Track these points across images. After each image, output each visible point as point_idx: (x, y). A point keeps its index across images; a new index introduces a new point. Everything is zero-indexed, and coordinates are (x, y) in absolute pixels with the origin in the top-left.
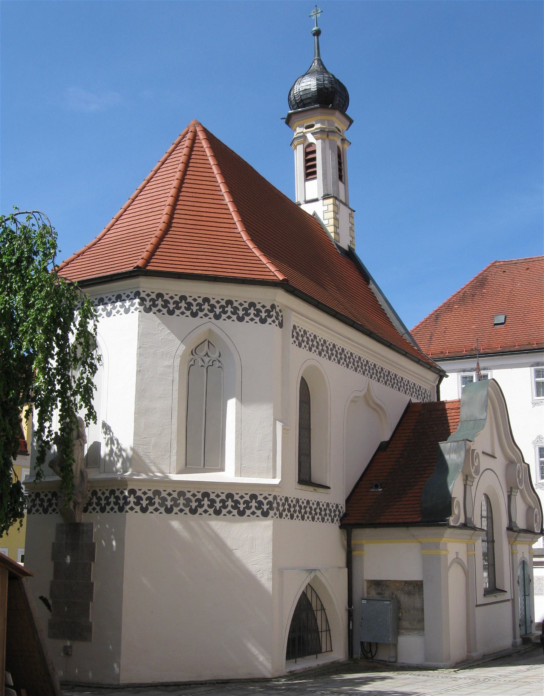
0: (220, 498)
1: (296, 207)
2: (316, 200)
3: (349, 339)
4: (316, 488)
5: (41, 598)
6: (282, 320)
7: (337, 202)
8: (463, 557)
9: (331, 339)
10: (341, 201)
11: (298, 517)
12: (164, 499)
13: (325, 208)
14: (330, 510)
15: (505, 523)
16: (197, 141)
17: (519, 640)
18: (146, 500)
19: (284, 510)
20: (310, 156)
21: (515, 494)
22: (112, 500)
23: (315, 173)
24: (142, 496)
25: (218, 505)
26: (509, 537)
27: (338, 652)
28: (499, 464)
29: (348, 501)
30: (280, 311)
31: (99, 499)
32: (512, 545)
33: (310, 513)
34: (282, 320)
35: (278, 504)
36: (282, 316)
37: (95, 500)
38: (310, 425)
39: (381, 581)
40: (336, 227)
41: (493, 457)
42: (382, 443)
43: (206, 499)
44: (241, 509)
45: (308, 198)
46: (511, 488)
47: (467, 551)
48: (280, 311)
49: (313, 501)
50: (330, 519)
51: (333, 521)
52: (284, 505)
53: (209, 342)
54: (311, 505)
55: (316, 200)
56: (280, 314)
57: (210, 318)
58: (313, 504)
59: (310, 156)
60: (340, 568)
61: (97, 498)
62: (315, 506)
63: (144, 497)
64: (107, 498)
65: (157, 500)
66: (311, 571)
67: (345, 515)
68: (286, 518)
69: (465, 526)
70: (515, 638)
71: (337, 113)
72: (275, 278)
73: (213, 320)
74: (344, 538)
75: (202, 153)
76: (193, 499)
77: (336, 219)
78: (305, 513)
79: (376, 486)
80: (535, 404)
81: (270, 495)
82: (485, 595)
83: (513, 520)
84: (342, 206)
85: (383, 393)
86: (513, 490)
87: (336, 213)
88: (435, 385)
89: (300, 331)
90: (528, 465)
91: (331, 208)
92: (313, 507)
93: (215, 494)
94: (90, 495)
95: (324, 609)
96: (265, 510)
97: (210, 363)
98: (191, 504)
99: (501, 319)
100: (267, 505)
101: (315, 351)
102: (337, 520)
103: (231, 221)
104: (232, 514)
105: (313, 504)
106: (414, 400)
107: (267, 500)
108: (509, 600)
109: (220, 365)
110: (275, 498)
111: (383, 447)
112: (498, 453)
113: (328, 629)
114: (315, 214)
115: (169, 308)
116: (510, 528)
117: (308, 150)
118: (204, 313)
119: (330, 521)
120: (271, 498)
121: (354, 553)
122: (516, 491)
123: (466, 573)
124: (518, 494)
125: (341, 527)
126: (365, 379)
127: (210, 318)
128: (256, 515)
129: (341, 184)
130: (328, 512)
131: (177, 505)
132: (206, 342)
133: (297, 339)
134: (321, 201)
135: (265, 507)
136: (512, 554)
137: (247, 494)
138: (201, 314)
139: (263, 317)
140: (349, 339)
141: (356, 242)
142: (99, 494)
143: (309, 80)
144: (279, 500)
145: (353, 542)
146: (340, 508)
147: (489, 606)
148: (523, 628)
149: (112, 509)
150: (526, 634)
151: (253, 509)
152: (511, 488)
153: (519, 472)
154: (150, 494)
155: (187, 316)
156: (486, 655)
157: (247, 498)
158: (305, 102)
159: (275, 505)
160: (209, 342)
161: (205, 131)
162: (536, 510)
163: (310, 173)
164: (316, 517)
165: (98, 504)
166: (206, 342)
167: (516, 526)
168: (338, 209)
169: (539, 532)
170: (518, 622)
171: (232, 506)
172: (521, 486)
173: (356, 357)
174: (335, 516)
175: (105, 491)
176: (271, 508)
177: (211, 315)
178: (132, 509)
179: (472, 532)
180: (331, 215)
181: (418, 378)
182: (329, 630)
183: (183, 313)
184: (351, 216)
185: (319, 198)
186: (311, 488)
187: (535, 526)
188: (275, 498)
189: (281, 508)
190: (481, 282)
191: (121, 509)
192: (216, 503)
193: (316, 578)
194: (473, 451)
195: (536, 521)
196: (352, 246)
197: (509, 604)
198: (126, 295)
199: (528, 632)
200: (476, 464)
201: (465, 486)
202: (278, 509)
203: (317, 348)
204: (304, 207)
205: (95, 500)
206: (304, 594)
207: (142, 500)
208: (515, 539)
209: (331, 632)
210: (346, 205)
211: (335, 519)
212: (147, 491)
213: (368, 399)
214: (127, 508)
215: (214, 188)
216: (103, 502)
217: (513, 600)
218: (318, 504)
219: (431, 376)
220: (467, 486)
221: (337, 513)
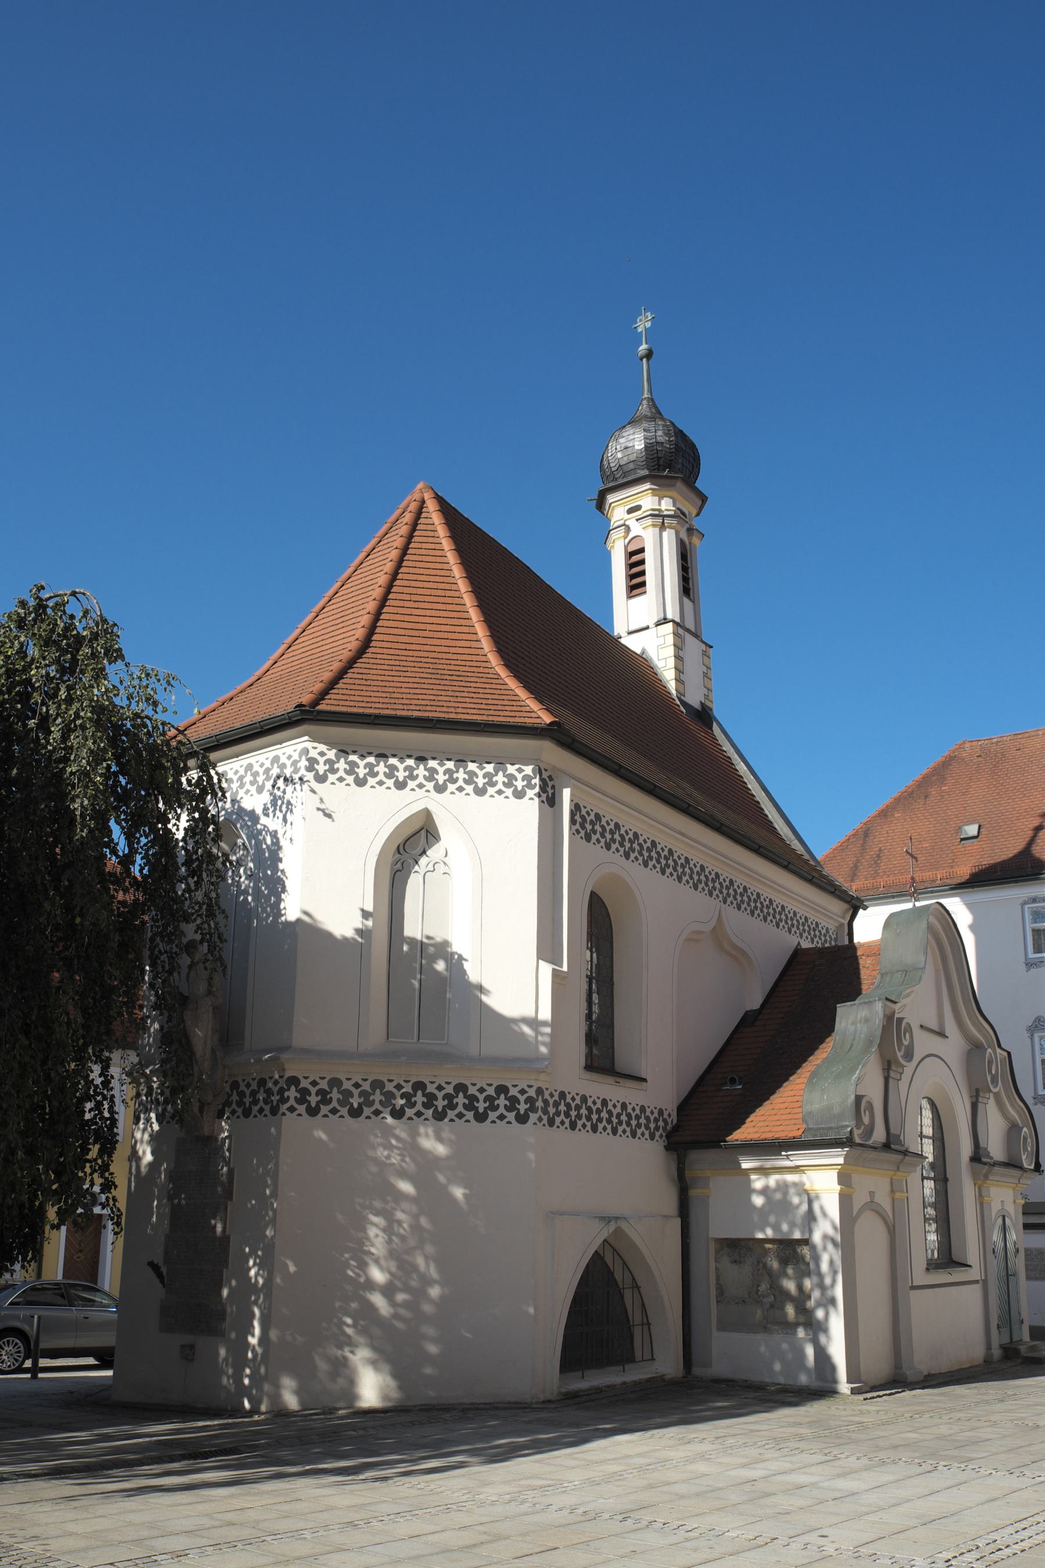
0: (444, 1092)
1: (615, 641)
2: (647, 628)
3: (683, 834)
4: (618, 1080)
5: (151, 1264)
6: (553, 794)
7: (681, 631)
8: (884, 1200)
9: (647, 832)
10: (688, 631)
11: (584, 1126)
12: (347, 1094)
13: (661, 641)
14: (647, 1118)
15: (966, 1150)
16: (423, 515)
17: (997, 1353)
18: (317, 1095)
19: (558, 1113)
20: (635, 558)
21: (985, 1101)
22: (261, 1096)
23: (643, 584)
24: (310, 1087)
25: (440, 1103)
26: (975, 1176)
27: (667, 1362)
28: (953, 1047)
29: (681, 1108)
30: (551, 778)
31: (242, 1095)
32: (980, 1188)
33: (609, 1121)
34: (553, 794)
35: (546, 1102)
36: (553, 787)
37: (235, 1097)
38: (612, 977)
39: (739, 1240)
40: (679, 670)
41: (942, 1034)
42: (747, 1012)
43: (419, 1093)
44: (481, 1110)
45: (632, 629)
46: (977, 1091)
47: (892, 1191)
48: (551, 778)
49: (614, 1101)
50: (647, 1133)
51: (652, 1137)
52: (556, 1104)
53: (427, 831)
54: (610, 1107)
55: (647, 628)
56: (550, 784)
57: (428, 791)
58: (615, 1106)
59: (635, 558)
60: (666, 1216)
61: (238, 1094)
62: (618, 1109)
63: (313, 1090)
64: (254, 1093)
65: (335, 1095)
66: (607, 1220)
67: (676, 1128)
68: (562, 1128)
69: (887, 1146)
70: (989, 1347)
71: (679, 484)
72: (538, 721)
73: (433, 792)
74: (674, 1167)
75: (432, 534)
76: (398, 1094)
77: (678, 658)
78: (600, 1120)
79: (733, 1081)
80: (1030, 965)
81: (530, 1086)
82: (927, 1269)
83: (982, 1144)
84: (689, 638)
85: (741, 924)
86: (981, 1094)
87: (678, 647)
88: (846, 922)
89: (588, 814)
90: (1009, 1054)
91: (670, 639)
92: (615, 1112)
93: (436, 1085)
94: (228, 1089)
95: (638, 1288)
96: (522, 1112)
97: (430, 867)
98: (393, 1102)
99: (972, 830)
100: (526, 1103)
101: (618, 850)
102: (661, 1136)
103: (474, 637)
104: (464, 1119)
105: (615, 1106)
106: (806, 944)
107: (526, 1096)
108: (976, 1282)
109: (446, 870)
110: (540, 1091)
111: (749, 1020)
112: (951, 1027)
113: (645, 1321)
114: (644, 651)
115: (357, 774)
116: (978, 1157)
117: (631, 549)
118: (417, 782)
119: (647, 1135)
120: (532, 1092)
121: (692, 1192)
122: (987, 1095)
123: (892, 1232)
124: (992, 1102)
125: (667, 1148)
126: (713, 904)
127: (428, 791)
128: (506, 1120)
129: (686, 600)
130: (643, 1121)
131: (371, 1104)
132: (423, 832)
133: (583, 826)
134: (652, 631)
135: (522, 1107)
136: (982, 1204)
137: (490, 1085)
138: (411, 784)
139: (520, 788)
140: (683, 834)
141: (714, 696)
142: (242, 1087)
143: (631, 432)
144: (547, 1096)
145: (687, 1173)
146: (666, 1116)
147: (936, 1290)
148: (1005, 1331)
149: (261, 1110)
150: (1011, 1342)
151: (502, 1110)
152: (977, 1091)
153: (990, 1063)
154: (324, 1085)
155: (389, 788)
156: (934, 1375)
157: (491, 1091)
158: (626, 469)
159: (540, 1104)
160: (427, 831)
161: (447, 511)
162: (1025, 1129)
163: (636, 585)
164: (620, 1129)
165: (240, 1103)
166: (423, 832)
167: (988, 1155)
168: (683, 641)
169: (1032, 1167)
170: (994, 1321)
171: (465, 1106)
172: (996, 1087)
173: (695, 866)
174: (657, 1128)
175: (251, 1082)
176: (533, 1109)
177: (430, 786)
178: (292, 1109)
179: (900, 1157)
180: (671, 651)
181: (812, 908)
182: (649, 1324)
183: (381, 783)
184: (704, 653)
185: (651, 625)
186: (610, 1080)
187: (1024, 1157)
188: (540, 1091)
189: (552, 1110)
190: (939, 773)
191: (274, 1111)
192: (436, 1099)
193: (618, 1232)
194: (900, 1020)
195: (1025, 1149)
196: (708, 703)
197: (978, 1287)
198: (287, 755)
199: (1015, 1339)
200: (906, 1043)
201: (886, 1080)
202: (545, 1111)
203: (622, 845)
204: (628, 641)
205: (235, 1097)
206: (597, 1258)
207: (310, 1095)
208: (986, 1177)
209: (652, 1327)
210: (696, 635)
211: (657, 1134)
212: (318, 1080)
213: (718, 934)
214: (284, 1108)
215: (448, 587)
216: (247, 1100)
217: (985, 1282)
218: (624, 1106)
219: (836, 907)
220: (891, 1080)
221: (661, 1123)
